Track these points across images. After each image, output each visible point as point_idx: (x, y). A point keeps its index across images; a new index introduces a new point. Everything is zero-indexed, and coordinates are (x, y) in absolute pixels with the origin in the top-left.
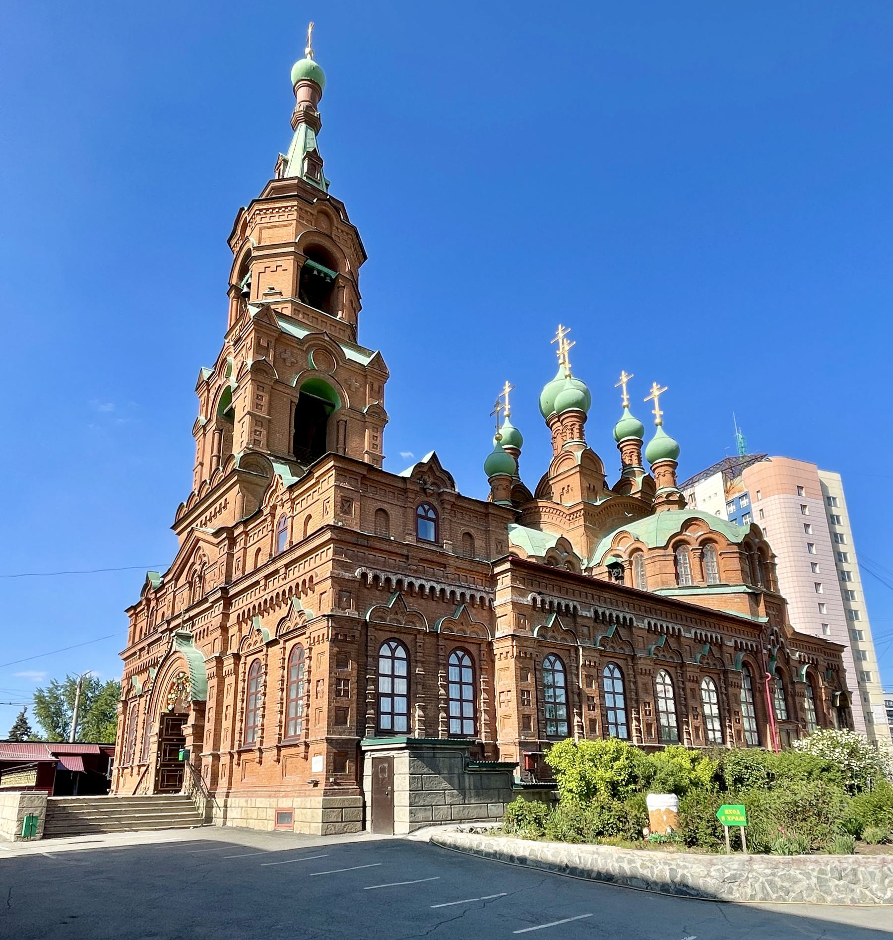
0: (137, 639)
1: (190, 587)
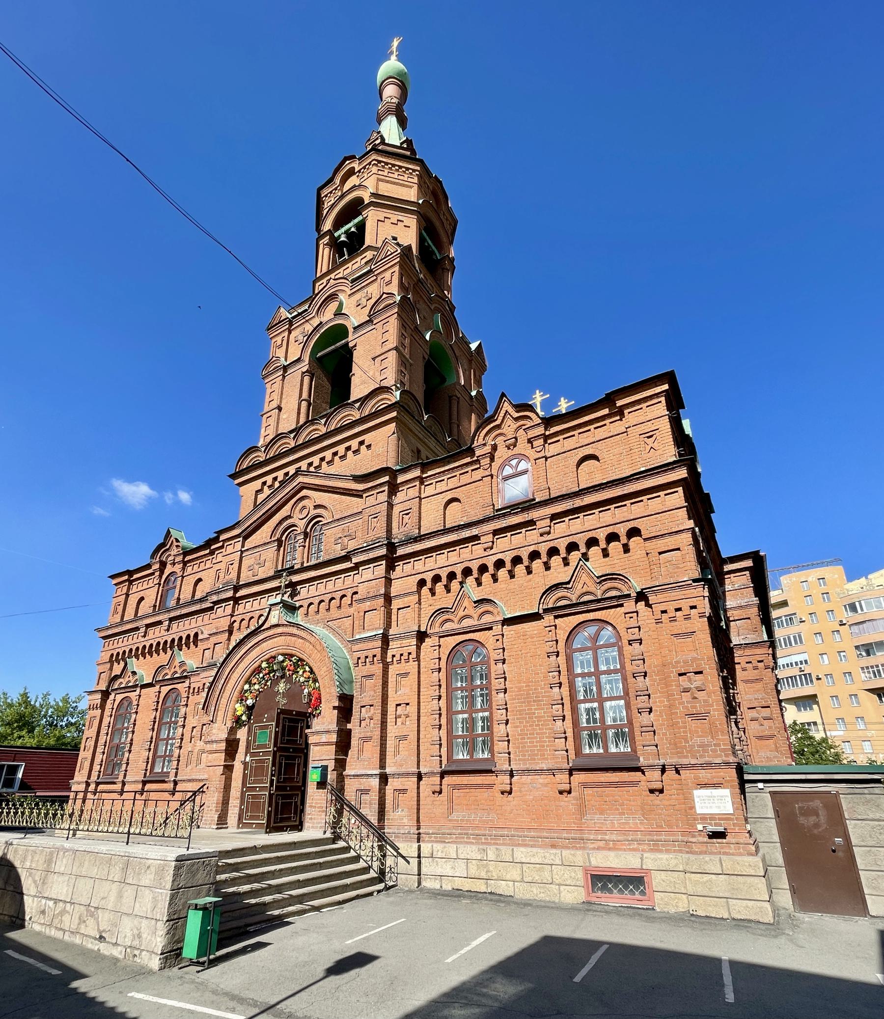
0: (130, 614)
1: (279, 546)
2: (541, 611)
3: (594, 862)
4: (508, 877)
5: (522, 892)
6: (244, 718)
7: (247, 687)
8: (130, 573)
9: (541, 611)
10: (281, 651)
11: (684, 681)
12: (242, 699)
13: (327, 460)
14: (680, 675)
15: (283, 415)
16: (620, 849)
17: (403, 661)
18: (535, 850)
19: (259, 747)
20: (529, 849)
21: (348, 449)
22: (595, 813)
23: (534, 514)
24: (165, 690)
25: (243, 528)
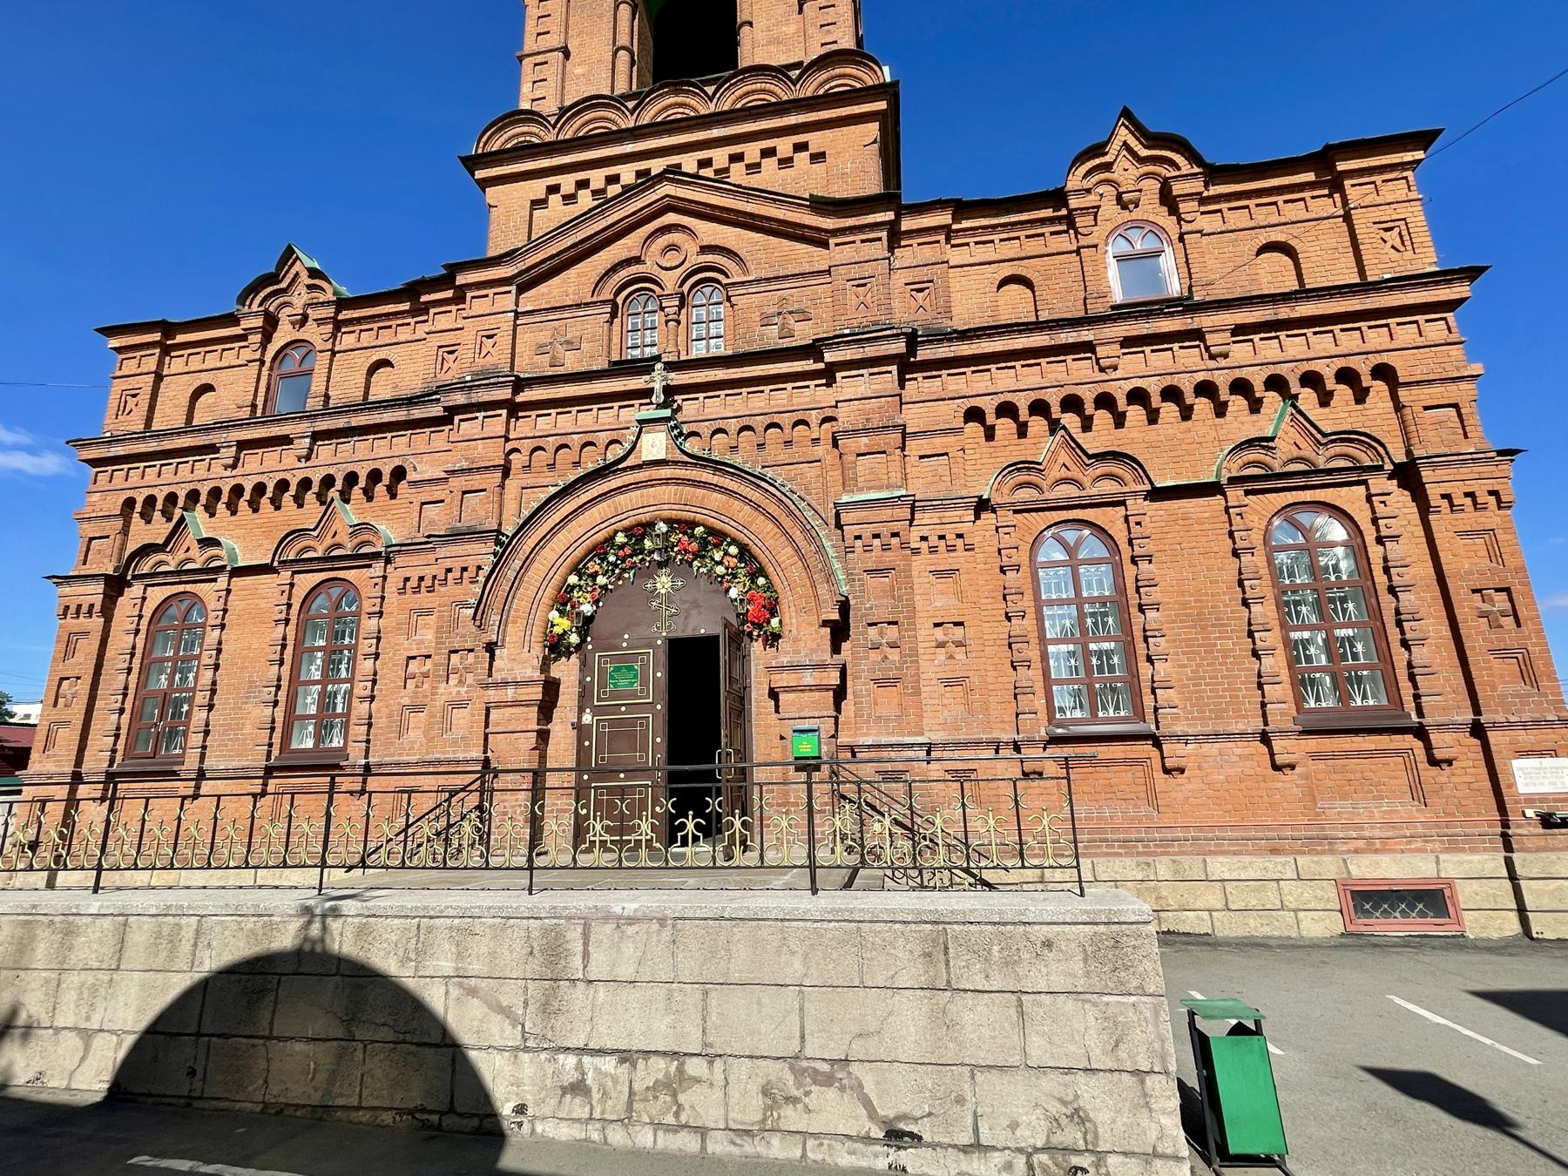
1: (614, 314)
2: (1224, 481)
3: (1356, 872)
4: (1199, 905)
5: (1228, 927)
6: (574, 639)
7: (573, 579)
8: (169, 329)
9: (1224, 481)
10: (666, 514)
11: (939, 632)
12: (563, 601)
13: (564, 190)
14: (936, 625)
15: (576, 68)
16: (1394, 851)
17: (423, 589)
18: (1247, 859)
19: (615, 695)
20: (1236, 859)
21: (553, 189)
22: (1333, 799)
23: (1204, 321)
24: (306, 582)
25: (522, 266)
